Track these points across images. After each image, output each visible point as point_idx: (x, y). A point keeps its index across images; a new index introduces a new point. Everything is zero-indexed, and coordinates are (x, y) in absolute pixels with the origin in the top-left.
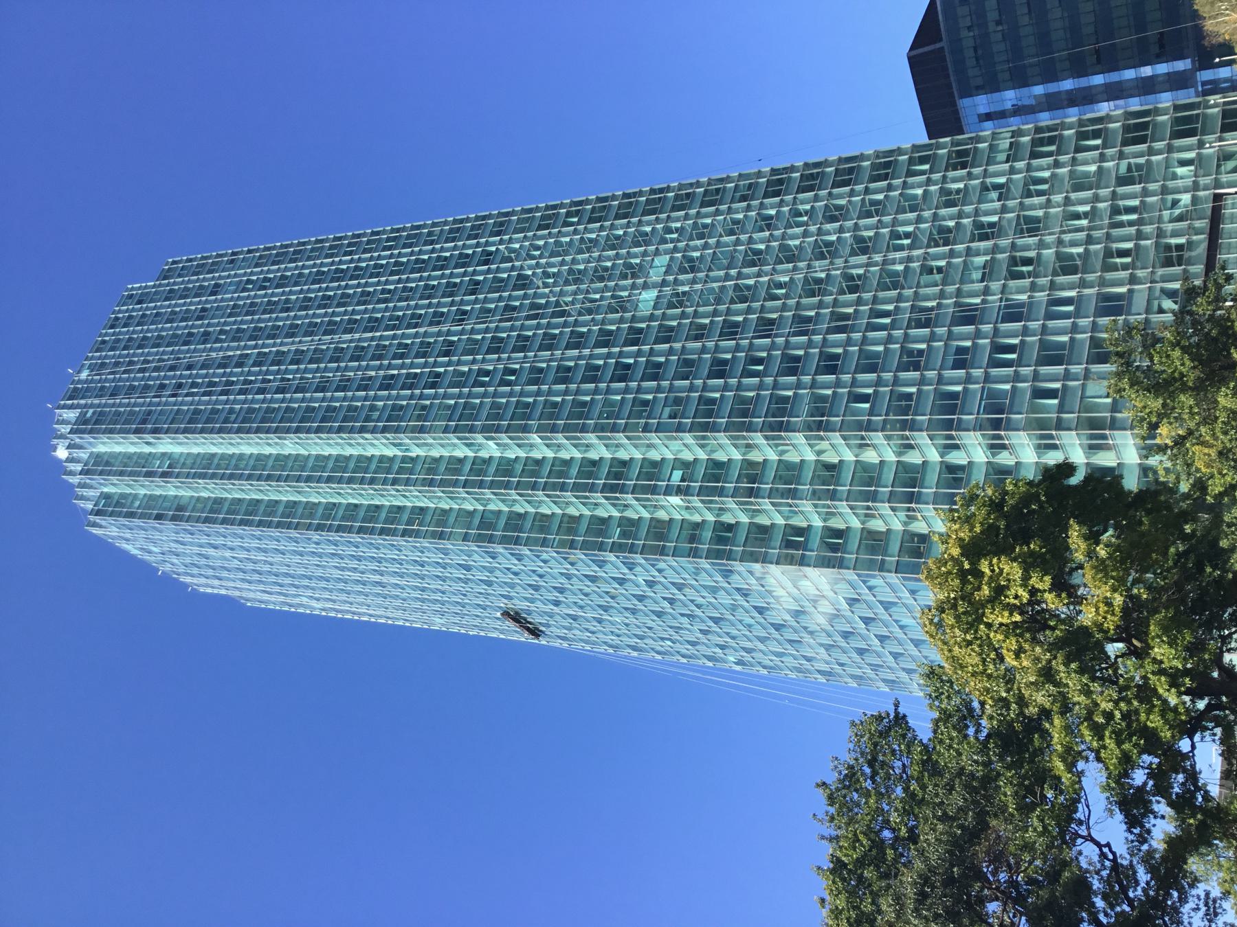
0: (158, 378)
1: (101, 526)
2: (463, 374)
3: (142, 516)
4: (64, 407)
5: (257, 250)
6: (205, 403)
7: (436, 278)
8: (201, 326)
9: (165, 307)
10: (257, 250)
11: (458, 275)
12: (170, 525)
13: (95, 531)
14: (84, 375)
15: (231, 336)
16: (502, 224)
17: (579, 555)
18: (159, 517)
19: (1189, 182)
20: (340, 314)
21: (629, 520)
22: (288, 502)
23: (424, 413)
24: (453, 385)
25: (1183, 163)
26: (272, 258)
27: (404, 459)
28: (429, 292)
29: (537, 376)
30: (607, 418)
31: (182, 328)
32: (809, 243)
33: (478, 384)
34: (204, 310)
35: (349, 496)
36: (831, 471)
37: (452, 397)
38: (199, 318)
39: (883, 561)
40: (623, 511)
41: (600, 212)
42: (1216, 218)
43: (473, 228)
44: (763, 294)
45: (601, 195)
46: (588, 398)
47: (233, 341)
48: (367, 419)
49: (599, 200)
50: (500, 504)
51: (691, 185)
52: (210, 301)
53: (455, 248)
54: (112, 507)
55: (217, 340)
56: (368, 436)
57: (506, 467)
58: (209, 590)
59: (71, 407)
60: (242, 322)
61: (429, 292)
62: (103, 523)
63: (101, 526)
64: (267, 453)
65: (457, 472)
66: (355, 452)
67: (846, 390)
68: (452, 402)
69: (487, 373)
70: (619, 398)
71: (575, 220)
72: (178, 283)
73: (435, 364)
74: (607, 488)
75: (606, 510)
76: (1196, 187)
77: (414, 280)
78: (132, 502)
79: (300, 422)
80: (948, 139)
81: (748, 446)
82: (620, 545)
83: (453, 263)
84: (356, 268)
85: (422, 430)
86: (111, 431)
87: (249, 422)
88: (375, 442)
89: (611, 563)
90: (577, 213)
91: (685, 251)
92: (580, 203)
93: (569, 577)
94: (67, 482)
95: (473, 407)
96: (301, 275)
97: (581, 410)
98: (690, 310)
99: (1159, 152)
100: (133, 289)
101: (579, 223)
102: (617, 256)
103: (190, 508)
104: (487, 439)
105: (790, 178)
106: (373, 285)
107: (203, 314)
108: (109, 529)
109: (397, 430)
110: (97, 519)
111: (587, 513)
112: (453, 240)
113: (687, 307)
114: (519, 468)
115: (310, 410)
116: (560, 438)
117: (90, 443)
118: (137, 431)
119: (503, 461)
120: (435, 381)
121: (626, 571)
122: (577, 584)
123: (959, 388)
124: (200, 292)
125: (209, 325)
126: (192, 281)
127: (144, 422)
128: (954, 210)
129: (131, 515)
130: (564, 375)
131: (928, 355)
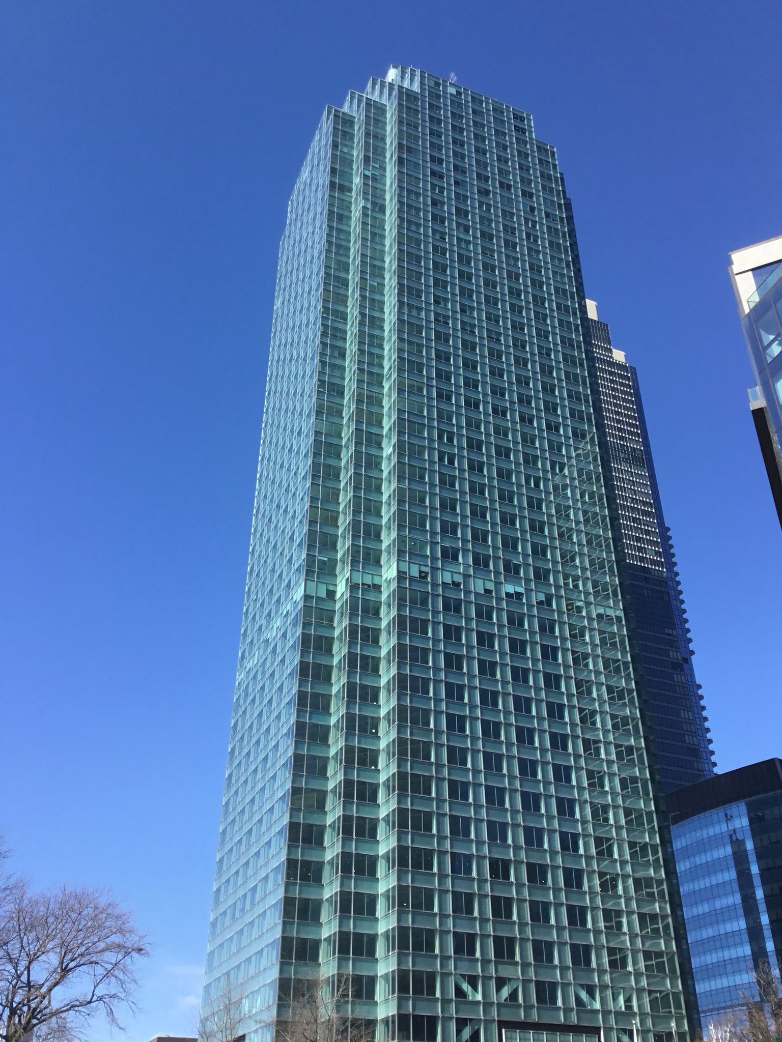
6: (427, 248)
7: (534, 387)
11: (537, 405)
13: (325, 113)
16: (579, 399)
18: (333, 171)
19: (611, 1006)
20: (503, 308)
23: (416, 390)
25: (628, 1000)
27: (381, 376)
28: (523, 381)
29: (447, 482)
31: (492, 170)
37: (429, 413)
39: (299, 810)
42: (577, 1030)
48: (410, 306)
52: (516, 193)
57: (374, 463)
59: (422, 83)
61: (523, 381)
62: (329, 121)
65: (368, 511)
66: (386, 353)
72: (533, 161)
76: (606, 1013)
77: (533, 368)
78: (346, 146)
81: (389, 606)
95: (421, 431)
101: (584, 503)
106: (530, 333)
107: (505, 187)
108: (326, 126)
117: (392, 104)
127: (409, 150)
129: (335, 146)
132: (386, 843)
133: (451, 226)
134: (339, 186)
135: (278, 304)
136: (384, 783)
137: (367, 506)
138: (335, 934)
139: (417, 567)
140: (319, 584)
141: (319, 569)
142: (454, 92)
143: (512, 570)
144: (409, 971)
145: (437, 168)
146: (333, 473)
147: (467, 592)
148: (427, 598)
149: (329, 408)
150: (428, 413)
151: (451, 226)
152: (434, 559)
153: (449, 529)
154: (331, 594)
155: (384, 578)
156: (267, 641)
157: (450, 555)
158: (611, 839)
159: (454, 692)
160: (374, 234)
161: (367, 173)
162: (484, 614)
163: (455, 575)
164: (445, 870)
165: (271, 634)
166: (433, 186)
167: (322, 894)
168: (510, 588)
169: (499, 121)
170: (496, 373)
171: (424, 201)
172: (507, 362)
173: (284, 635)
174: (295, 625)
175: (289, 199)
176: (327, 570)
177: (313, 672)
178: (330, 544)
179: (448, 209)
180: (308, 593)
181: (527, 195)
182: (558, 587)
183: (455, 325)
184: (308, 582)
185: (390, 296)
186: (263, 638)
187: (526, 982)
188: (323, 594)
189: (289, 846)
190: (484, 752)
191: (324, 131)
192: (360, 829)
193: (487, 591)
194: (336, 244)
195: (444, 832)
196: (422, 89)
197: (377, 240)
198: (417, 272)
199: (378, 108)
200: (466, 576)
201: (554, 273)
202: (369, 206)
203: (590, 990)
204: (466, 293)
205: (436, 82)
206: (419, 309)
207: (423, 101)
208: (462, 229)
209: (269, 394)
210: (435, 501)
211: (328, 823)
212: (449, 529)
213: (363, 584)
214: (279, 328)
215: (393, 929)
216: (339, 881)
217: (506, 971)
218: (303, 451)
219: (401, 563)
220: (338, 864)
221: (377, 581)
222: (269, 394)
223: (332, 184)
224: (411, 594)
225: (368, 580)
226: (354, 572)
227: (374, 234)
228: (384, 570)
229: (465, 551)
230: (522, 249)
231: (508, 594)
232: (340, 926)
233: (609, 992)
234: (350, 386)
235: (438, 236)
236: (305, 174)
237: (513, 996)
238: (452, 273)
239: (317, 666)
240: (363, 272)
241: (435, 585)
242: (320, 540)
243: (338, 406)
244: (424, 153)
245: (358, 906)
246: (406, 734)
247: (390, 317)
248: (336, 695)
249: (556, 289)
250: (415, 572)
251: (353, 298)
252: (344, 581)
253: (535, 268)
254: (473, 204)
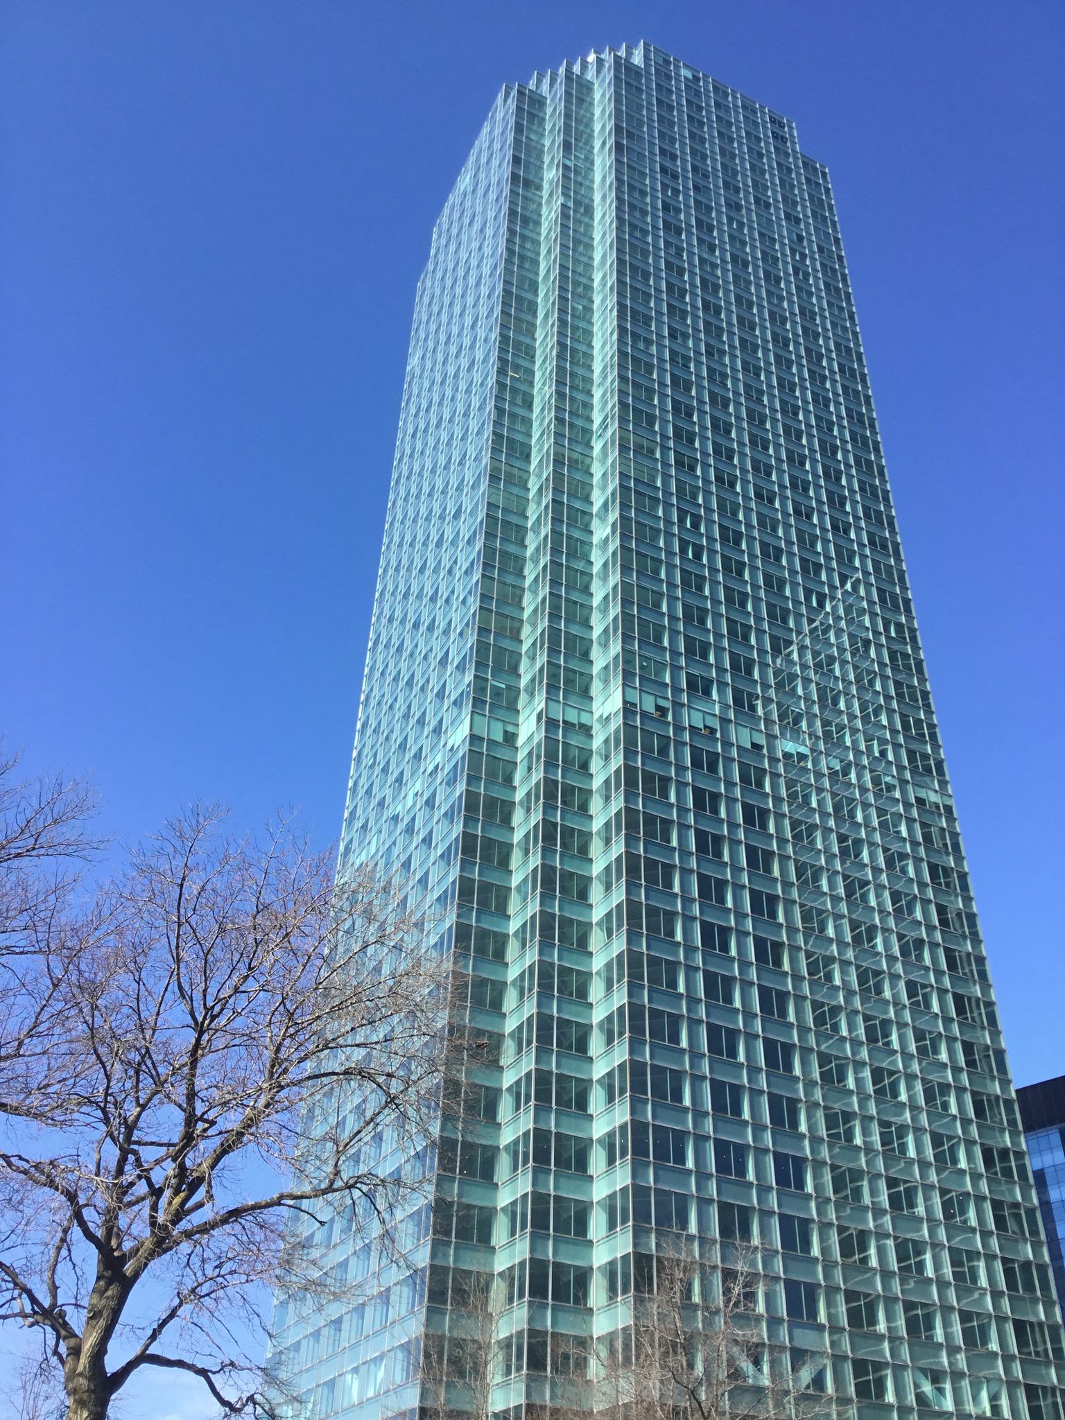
0: (683, 152)
1: (505, 100)
3: (517, 142)
4: (647, 50)
5: (842, 266)
6: (657, 262)
8: (747, 201)
10: (842, 266)
11: (817, 494)
12: (507, 172)
13: (501, 96)
14: (685, 72)
15: (736, 234)
16: (884, 547)
17: (472, 638)
18: (516, 160)
20: (766, 357)
22: (534, 349)
23: (645, 452)
25: (994, 1398)
27: (587, 432)
28: (796, 460)
29: (692, 583)
30: (642, 667)
32: (853, 793)
33: (682, 514)
34: (768, 206)
36: (579, 891)
37: (665, 482)
38: (757, 200)
40: (526, 690)
41: (904, 662)
43: (878, 513)
45: (896, 521)
46: (666, 643)
50: (530, 642)
51: (928, 705)
52: (778, 213)
56: (615, 337)
57: (579, 550)
58: (434, 237)
59: (646, 57)
61: (796, 460)
62: (510, 101)
63: (505, 100)
68: (659, 484)
69: (696, 525)
70: (668, 680)
71: (893, 634)
72: (799, 177)
74: (550, 784)
80: (1047, 1258)
82: (484, 689)
83: (833, 488)
85: (623, 448)
86: (618, 101)
87: (631, 270)
88: (608, 346)
89: (447, 873)
91: (857, 765)
92: (914, 639)
93: (446, 632)
94: (560, 64)
96: (810, 294)
99: (1007, 1370)
100: (791, 128)
101: (888, 637)
103: (527, 233)
105: (926, 742)
106: (803, 395)
108: (503, 110)
109: (623, 420)
110: (514, 93)
112: (862, 489)
114: (580, 565)
116: (615, 610)
117: (603, 80)
118: (618, 128)
120: (685, 465)
121: (453, 698)
124: (790, 202)
127: (630, 135)
128: (921, 1101)
129: (519, 128)
131: (730, 1064)
132: (606, 1118)
134: (523, 178)
135: (413, 362)
136: (601, 1024)
137: (568, 606)
138: (522, 1264)
141: (493, 697)
142: (690, 76)
143: (790, 722)
144: (650, 1188)
145: (668, 164)
146: (515, 565)
147: (727, 744)
148: (668, 745)
149: (508, 475)
152: (677, 690)
153: (697, 650)
154: (510, 738)
155: (596, 716)
156: (395, 818)
157: (699, 687)
158: (954, 1138)
159: (711, 890)
162: (751, 778)
164: (706, 1166)
165: (407, 803)
166: (665, 187)
167: (495, 1199)
169: (751, 121)
170: (759, 443)
171: (653, 202)
172: (774, 429)
173: (430, 803)
174: (451, 782)
176: (506, 703)
177: (482, 851)
179: (687, 217)
180: (475, 732)
181: (792, 219)
182: (858, 753)
183: (698, 370)
187: (838, 1359)
188: (499, 737)
189: (429, 1309)
192: (560, 1094)
193: (756, 747)
194: (519, 254)
195: (699, 1047)
196: (647, 64)
197: (581, 249)
200: (724, 721)
201: (834, 324)
202: (571, 204)
203: (936, 1377)
206: (648, 342)
207: (649, 80)
209: (385, 571)
210: (677, 642)
211: (505, 1085)
212: (697, 650)
215: (625, 1258)
216: (530, 1174)
217: (806, 1339)
220: (524, 1215)
221: (585, 719)
222: (385, 571)
223: (515, 178)
224: (643, 735)
225: (572, 717)
226: (551, 703)
227: (577, 242)
228: (595, 705)
230: (789, 286)
231: (787, 756)
232: (532, 1250)
233: (965, 1383)
235: (672, 251)
237: (818, 1381)
238: (693, 300)
240: (562, 289)
241: (679, 728)
242: (493, 657)
244: (652, 144)
245: (557, 1219)
249: (837, 345)
250: (649, 705)
252: (534, 717)
253: (807, 313)
254: (719, 216)
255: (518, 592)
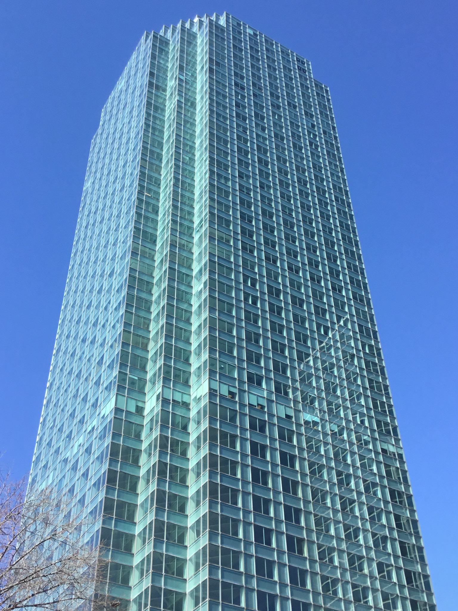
1: (146, 40)
2: (253, 268)
7: (321, 254)
8: (284, 104)
9: (296, 83)
10: (345, 186)
11: (323, 269)
12: (146, 80)
15: (277, 122)
16: (362, 301)
17: (118, 349)
18: (152, 74)
21: (144, 387)
22: (158, 207)
23: (224, 241)
24: (245, 261)
26: (338, 185)
27: (190, 229)
29: (252, 318)
33: (246, 278)
34: (295, 107)
35: (164, 203)
40: (150, 381)
44: (316, 486)
47: (274, 123)
49: (382, 369)
53: (343, 268)
54: (160, 46)
55: (274, 114)
56: (208, 175)
60: (293, 175)
62: (148, 41)
64: (195, 178)
67: (242, 549)
71: (367, 351)
73: (259, 250)
75: (151, 370)
78: (163, 59)
79: (218, 188)
82: (124, 380)
84: (327, 204)
85: (212, 238)
86: (211, 44)
88: (203, 180)
89: (112, 373)
90: (372, 354)
92: (379, 355)
93: (102, 345)
96: (319, 157)
97: (226, 350)
98: (306, 455)
100: (308, 65)
101: (365, 353)
102: (359, 494)
104: (205, 283)
105: (383, 395)
106: (315, 213)
109: (211, 222)
110: (151, 36)
111: (150, 355)
113: (311, 478)
114: (184, 306)
115: (226, 167)
116: (205, 333)
118: (211, 60)
119: (190, 231)
120: (248, 249)
121: (105, 385)
122: (96, 352)
123: (242, 569)
125: (284, 109)
126: (314, 101)
127: (218, 64)
129: (153, 57)
130: (253, 338)
133: (251, 124)
134: (155, 85)
135: (88, 185)
136: (192, 593)
139: (226, 387)
140: (129, 400)
141: (130, 385)
142: (252, 33)
150: (236, 295)
151: (251, 124)
152: (241, 382)
153: (253, 358)
154: (140, 410)
155: (193, 397)
157: (255, 381)
160: (186, 105)
161: (181, 77)
162: (286, 436)
163: (259, 398)
165: (74, 450)
168: (309, 417)
171: (230, 102)
172: (299, 231)
173: (88, 451)
175: (102, 107)
176: (137, 388)
178: (140, 365)
179: (249, 111)
180: (118, 406)
183: (256, 196)
184: (119, 397)
185: (201, 168)
186: (61, 458)
188: (133, 410)
190: (293, 601)
191: (142, 49)
193: (288, 417)
198: (224, 152)
199: (191, 35)
202: (183, 101)
204: (264, 175)
205: (238, 23)
206: (227, 179)
208: (260, 128)
212: (253, 358)
213: (173, 400)
214: (73, 288)
218: (107, 361)
219: (213, 382)
221: (186, 399)
222: (66, 307)
223: (151, 84)
224: (221, 409)
225: (178, 397)
226: (165, 389)
227: (186, 122)
228: (192, 390)
229: (268, 379)
230: (306, 152)
231: (307, 423)
234: (159, 273)
235: (241, 129)
236: (121, 84)
238: (253, 157)
239: (119, 535)
241: (242, 405)
243: (151, 251)
246: (217, 541)
247: (198, 287)
248: (142, 505)
250: (224, 390)
251: (161, 269)
252: (155, 397)
253: (317, 167)
254: (268, 112)
255: (147, 321)
